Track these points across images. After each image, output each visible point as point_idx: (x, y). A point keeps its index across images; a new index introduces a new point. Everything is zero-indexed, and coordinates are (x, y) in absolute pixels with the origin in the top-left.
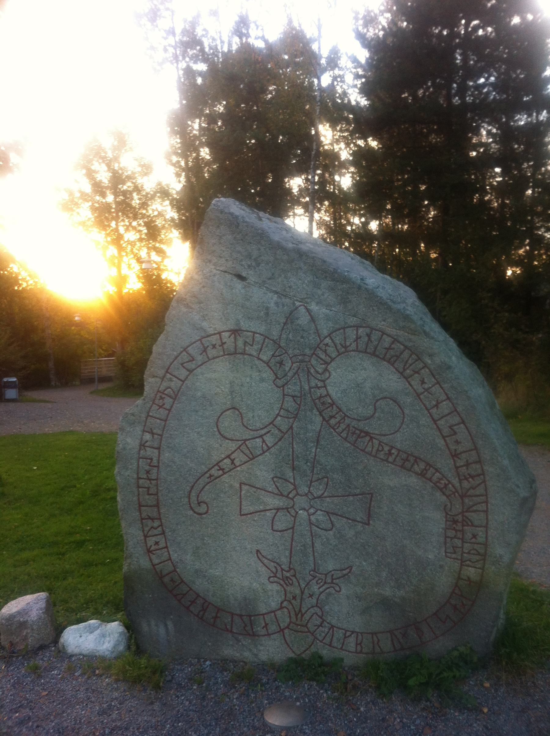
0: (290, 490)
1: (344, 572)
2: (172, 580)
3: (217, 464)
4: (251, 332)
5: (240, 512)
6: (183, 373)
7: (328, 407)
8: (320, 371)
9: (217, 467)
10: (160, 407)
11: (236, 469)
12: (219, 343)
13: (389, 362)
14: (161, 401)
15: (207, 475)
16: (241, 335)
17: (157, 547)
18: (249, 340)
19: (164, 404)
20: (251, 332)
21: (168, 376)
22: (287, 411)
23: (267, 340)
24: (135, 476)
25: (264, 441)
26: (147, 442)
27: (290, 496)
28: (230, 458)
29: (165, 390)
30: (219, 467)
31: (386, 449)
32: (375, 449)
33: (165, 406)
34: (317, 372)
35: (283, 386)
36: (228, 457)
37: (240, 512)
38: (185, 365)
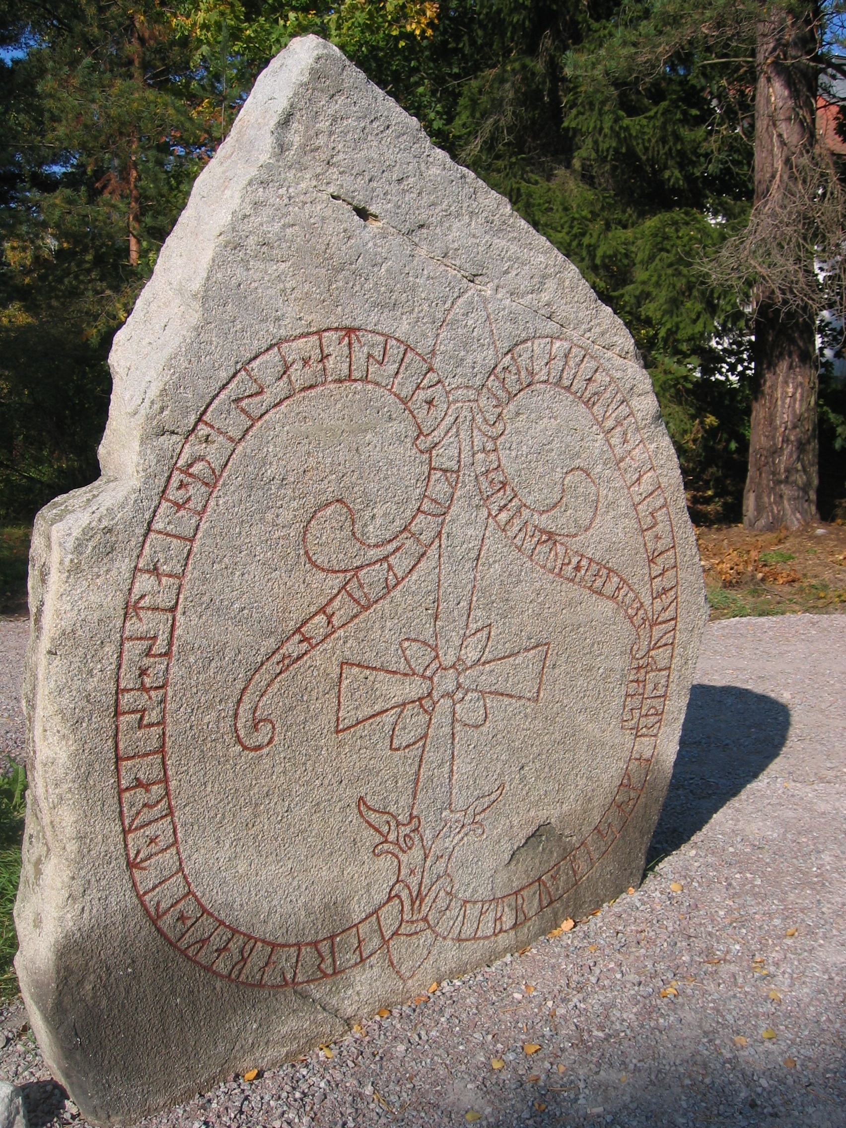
0: (427, 663)
1: (493, 797)
2: (182, 918)
3: (298, 630)
4: (382, 335)
5: (391, 745)
6: (234, 424)
7: (499, 490)
8: (492, 419)
9: (297, 637)
10: (179, 506)
11: (336, 635)
12: (316, 354)
13: (586, 403)
14: (182, 491)
15: (277, 657)
16: (363, 340)
17: (154, 848)
18: (377, 353)
19: (189, 499)
20: (382, 335)
21: (203, 430)
22: (434, 501)
23: (410, 355)
24: (112, 686)
25: (390, 568)
26: (142, 597)
27: (428, 673)
28: (324, 613)
29: (190, 466)
30: (303, 635)
31: (575, 561)
32: (559, 562)
33: (191, 505)
34: (485, 420)
35: (429, 450)
36: (322, 610)
37: (391, 745)
38: (243, 404)
